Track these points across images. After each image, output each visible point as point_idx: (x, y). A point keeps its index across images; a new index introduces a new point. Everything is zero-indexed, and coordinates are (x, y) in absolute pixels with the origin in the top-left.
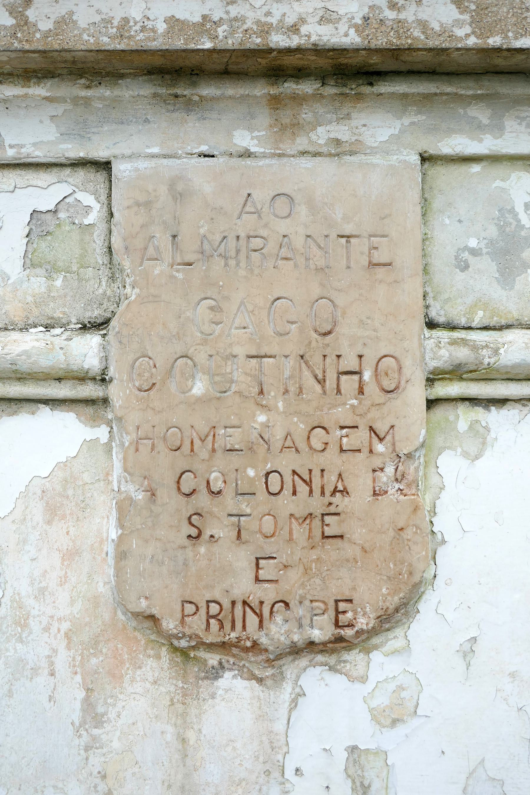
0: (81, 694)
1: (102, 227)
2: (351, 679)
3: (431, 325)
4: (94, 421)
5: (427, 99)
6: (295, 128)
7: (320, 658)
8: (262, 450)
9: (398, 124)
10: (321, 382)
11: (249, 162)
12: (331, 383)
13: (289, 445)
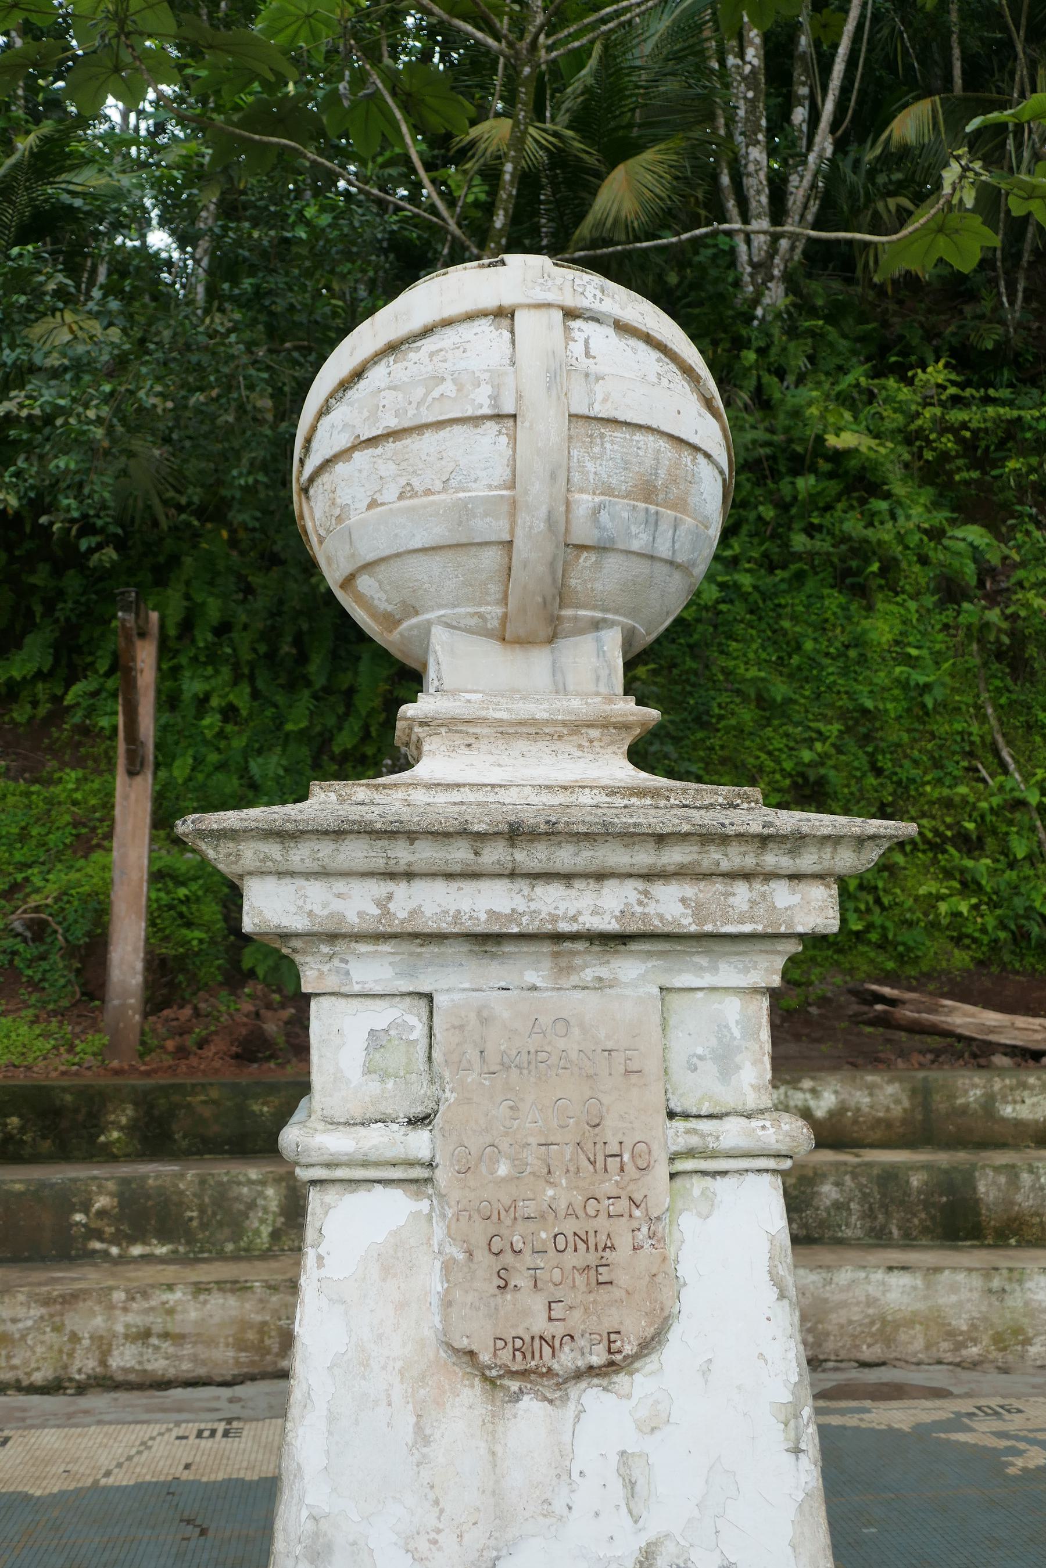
0: (413, 1420)
1: (425, 1042)
2: (620, 1396)
3: (671, 1115)
4: (418, 1196)
5: (662, 954)
6: (570, 969)
7: (596, 1381)
8: (551, 1217)
9: (643, 967)
10: (593, 1163)
11: (535, 994)
12: (600, 1164)
13: (571, 1213)
